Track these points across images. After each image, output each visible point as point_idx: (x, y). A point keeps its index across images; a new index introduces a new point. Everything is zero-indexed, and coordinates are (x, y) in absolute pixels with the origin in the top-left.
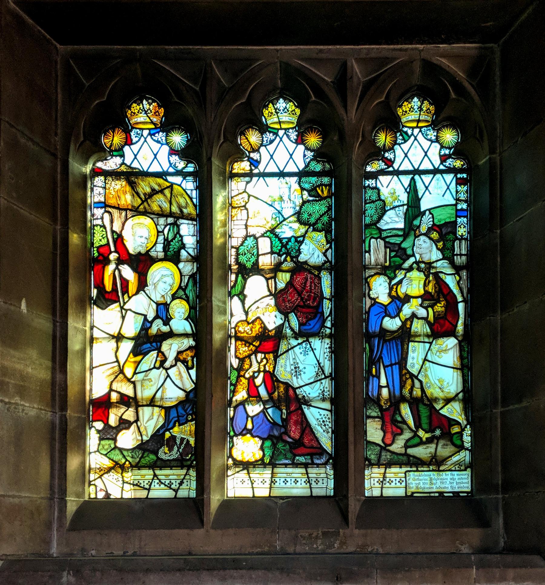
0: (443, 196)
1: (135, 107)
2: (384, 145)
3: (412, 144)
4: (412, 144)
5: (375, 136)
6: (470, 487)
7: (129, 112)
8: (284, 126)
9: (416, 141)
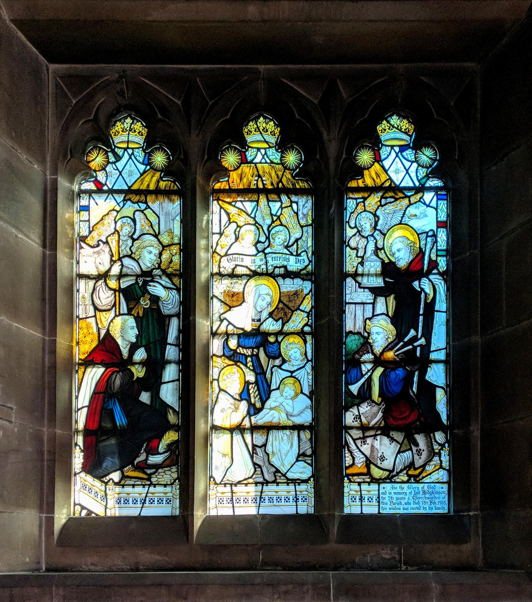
0: (97, 205)
1: (252, 126)
2: (431, 159)
3: (394, 160)
4: (394, 160)
5: (357, 152)
6: (446, 507)
7: (246, 130)
8: (131, 146)
9: (130, 160)
